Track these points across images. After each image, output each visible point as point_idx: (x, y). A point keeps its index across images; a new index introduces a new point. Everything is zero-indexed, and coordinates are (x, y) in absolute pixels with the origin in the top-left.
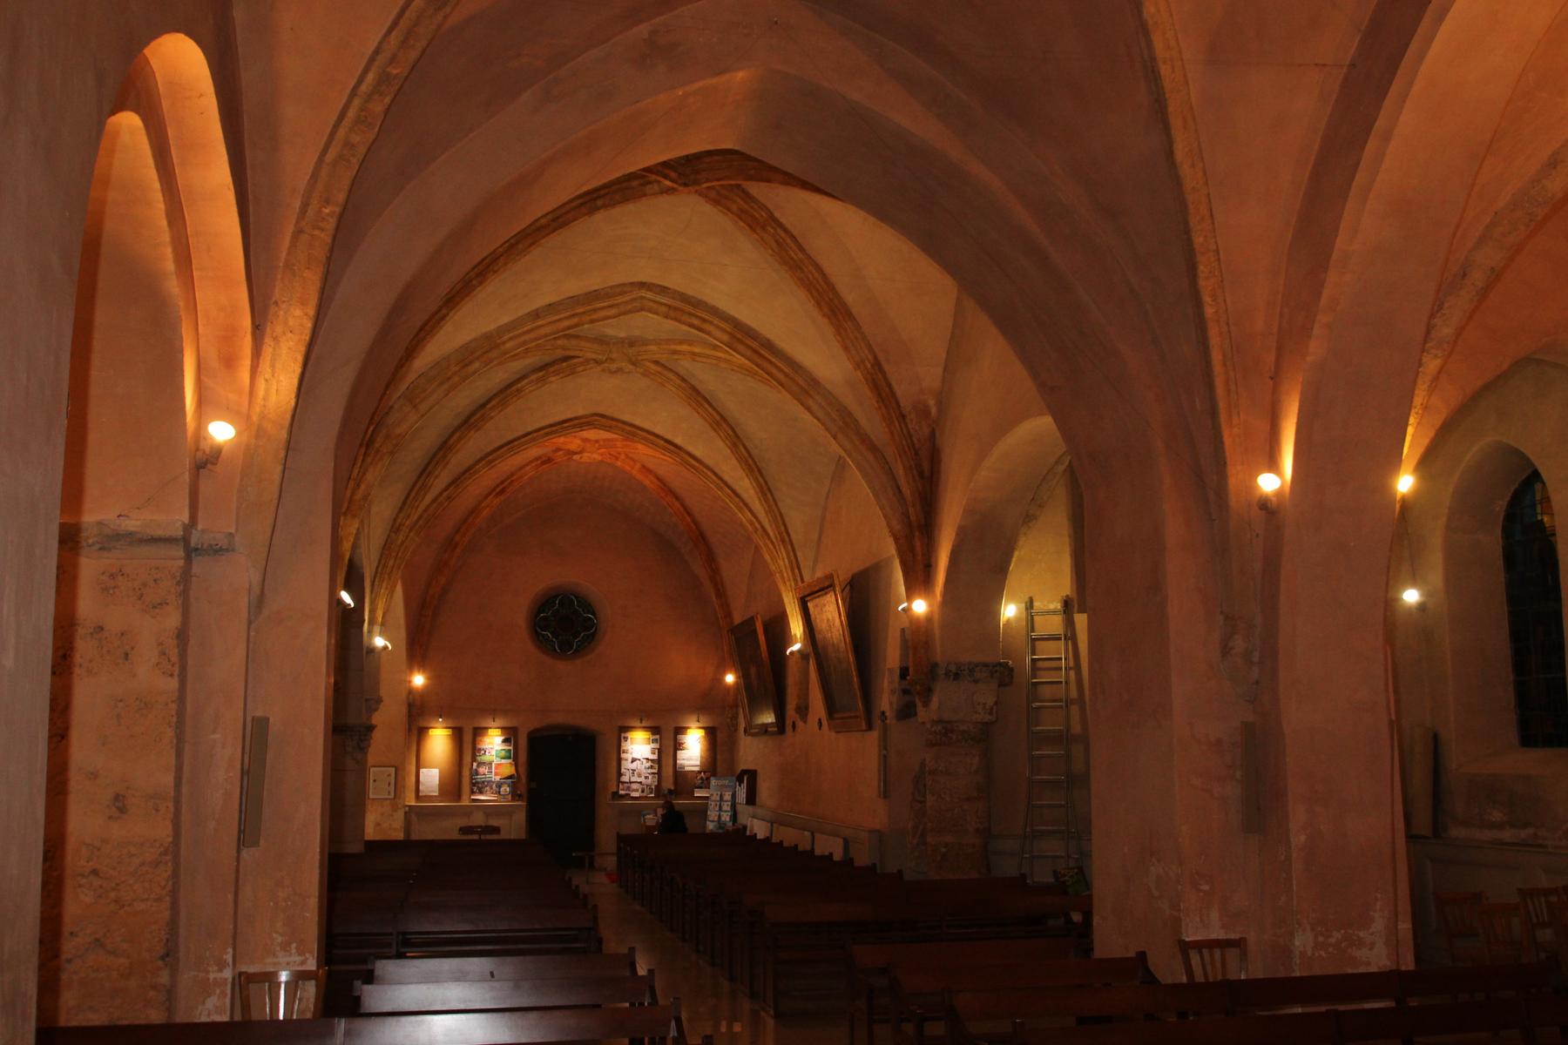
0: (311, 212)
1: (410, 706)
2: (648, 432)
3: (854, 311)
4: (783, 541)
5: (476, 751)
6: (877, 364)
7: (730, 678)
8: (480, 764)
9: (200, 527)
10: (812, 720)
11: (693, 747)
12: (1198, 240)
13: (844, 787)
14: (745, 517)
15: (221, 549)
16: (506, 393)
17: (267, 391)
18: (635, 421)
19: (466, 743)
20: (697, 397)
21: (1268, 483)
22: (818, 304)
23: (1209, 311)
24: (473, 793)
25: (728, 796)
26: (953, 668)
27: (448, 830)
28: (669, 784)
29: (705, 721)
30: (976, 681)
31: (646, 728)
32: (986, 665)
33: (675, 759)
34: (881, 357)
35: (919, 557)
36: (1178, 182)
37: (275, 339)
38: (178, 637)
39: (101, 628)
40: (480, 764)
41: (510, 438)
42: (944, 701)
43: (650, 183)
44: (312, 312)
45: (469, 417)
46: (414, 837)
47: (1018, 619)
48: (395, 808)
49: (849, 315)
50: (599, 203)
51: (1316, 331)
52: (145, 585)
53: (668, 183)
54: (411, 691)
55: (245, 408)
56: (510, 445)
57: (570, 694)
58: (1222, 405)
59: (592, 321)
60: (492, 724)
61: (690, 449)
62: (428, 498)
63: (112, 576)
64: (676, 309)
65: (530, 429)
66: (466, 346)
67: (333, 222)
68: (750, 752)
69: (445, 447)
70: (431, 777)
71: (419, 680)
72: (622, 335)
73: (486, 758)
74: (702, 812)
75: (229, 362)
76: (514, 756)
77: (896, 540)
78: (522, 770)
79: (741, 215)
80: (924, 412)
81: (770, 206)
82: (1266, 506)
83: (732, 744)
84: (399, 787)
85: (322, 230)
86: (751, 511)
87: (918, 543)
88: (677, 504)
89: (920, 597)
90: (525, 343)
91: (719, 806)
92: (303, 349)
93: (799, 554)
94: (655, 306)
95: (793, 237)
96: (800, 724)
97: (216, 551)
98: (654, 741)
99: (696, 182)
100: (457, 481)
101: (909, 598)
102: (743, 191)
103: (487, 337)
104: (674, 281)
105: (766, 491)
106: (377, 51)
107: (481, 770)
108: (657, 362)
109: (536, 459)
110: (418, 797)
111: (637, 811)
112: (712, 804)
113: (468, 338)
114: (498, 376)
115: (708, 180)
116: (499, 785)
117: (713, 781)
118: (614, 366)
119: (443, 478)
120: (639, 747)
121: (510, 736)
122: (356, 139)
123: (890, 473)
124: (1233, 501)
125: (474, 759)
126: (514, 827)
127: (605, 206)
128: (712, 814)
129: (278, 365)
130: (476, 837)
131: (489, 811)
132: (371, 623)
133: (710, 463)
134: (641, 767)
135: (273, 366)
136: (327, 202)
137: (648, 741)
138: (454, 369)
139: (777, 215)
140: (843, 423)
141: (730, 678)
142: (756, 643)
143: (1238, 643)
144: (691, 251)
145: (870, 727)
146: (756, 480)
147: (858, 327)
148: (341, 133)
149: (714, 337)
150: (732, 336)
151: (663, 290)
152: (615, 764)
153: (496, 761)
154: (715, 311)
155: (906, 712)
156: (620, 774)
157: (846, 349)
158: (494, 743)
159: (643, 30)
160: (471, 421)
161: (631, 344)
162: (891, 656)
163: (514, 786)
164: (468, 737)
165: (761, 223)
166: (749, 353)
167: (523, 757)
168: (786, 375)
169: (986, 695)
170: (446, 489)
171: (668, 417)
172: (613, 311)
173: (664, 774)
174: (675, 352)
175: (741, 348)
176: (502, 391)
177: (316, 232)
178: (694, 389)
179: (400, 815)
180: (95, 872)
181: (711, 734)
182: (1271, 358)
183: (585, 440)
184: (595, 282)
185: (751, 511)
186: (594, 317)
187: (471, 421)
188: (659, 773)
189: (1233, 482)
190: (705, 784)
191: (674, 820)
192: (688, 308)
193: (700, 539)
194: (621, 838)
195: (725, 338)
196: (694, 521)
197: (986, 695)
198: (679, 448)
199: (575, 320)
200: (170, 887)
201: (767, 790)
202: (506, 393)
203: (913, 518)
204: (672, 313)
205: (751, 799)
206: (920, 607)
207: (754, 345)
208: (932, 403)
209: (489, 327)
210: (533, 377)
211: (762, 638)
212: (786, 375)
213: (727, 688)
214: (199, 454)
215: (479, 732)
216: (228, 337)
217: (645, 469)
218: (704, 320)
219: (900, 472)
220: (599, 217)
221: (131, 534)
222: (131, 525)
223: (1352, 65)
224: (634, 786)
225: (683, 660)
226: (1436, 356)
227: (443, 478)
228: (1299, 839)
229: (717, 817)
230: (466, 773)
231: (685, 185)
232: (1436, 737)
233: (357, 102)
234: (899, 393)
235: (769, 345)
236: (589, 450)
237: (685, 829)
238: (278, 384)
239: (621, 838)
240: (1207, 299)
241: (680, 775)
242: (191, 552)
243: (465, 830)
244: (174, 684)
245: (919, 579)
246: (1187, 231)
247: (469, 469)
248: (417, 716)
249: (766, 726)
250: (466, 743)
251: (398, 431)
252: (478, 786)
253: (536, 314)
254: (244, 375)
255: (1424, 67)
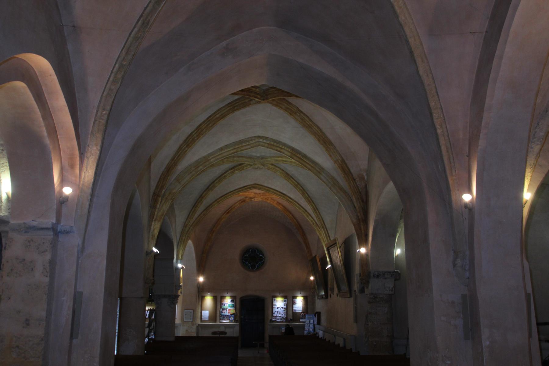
0: (99, 113)
5: (221, 304)
6: (343, 161)
7: (312, 278)
8: (223, 309)
10: (335, 294)
11: (299, 303)
12: (432, 104)
13: (344, 318)
14: (309, 219)
16: (221, 177)
17: (85, 176)
18: (268, 186)
19: (218, 301)
20: (288, 176)
21: (467, 198)
22: (319, 140)
23: (439, 131)
24: (220, 319)
25: (312, 322)
26: (376, 273)
27: (207, 333)
28: (290, 317)
29: (303, 294)
30: (385, 278)
31: (282, 296)
32: (390, 272)
34: (345, 159)
35: (363, 232)
36: (422, 83)
37: (87, 158)
38: (50, 263)
39: (24, 260)
40: (223, 309)
41: (225, 193)
42: (375, 286)
43: (252, 100)
44: (99, 148)
45: (208, 187)
46: (200, 335)
47: (401, 254)
48: (193, 325)
49: (331, 144)
50: (236, 108)
51: (482, 136)
52: (40, 245)
53: (257, 99)
54: (199, 283)
55: (78, 183)
56: (225, 196)
57: (255, 284)
58: (447, 168)
59: (242, 150)
60: (299, 295)
61: (289, 195)
62: (196, 215)
63: (29, 242)
64: (271, 145)
65: (232, 190)
66: (197, 161)
67: (106, 116)
68: (320, 305)
69: (201, 197)
70: (206, 314)
71: (201, 279)
72: (258, 155)
73: (225, 307)
74: (303, 327)
75: (72, 166)
76: (235, 306)
77: (354, 225)
78: (238, 311)
79: (286, 110)
80: (362, 178)
81: (297, 106)
82: (466, 206)
83: (314, 303)
84: (194, 317)
85: (102, 119)
86: (311, 217)
87: (362, 227)
88: (291, 215)
89: (363, 247)
90: (217, 159)
91: (309, 325)
92: (96, 161)
93: (329, 232)
94: (263, 144)
95: (307, 116)
96: (332, 295)
97: (67, 232)
98: (285, 301)
99: (267, 99)
100: (207, 208)
101: (360, 248)
102: (287, 101)
103: (204, 157)
104: (269, 135)
105: (316, 209)
106: (119, 57)
107: (223, 311)
108: (272, 164)
109: (240, 201)
110: (201, 321)
111: (279, 327)
112: (306, 325)
113: (197, 158)
114: (217, 171)
115: (271, 98)
117: (307, 316)
118: (256, 166)
119: (201, 209)
120: (279, 303)
121: (233, 299)
122: (113, 87)
123: (351, 201)
124: (454, 205)
125: (221, 308)
126: (234, 332)
127: (237, 109)
128: (306, 329)
129: (89, 167)
130: (218, 336)
131: (226, 326)
132: (177, 259)
133: (295, 200)
134: (280, 310)
135: (87, 167)
136: (104, 110)
138: (193, 169)
139: (300, 109)
140: (333, 183)
141: (312, 278)
142: (316, 264)
143: (459, 262)
144: (267, 122)
145: (351, 296)
146: (312, 205)
149: (282, 154)
150: (292, 153)
151: (266, 138)
152: (271, 309)
153: (229, 308)
154: (285, 145)
155: (362, 291)
156: (273, 313)
157: (330, 156)
159: (224, 44)
160: (210, 187)
161: (262, 158)
162: (357, 269)
163: (235, 317)
164: (219, 299)
165: (295, 112)
166: (298, 159)
167: (238, 306)
168: (312, 167)
169: (390, 284)
170: (203, 212)
171: (279, 184)
172: (249, 147)
173: (289, 313)
174: (277, 160)
175: (295, 158)
176: (220, 177)
177: (101, 120)
178: (288, 174)
179: (195, 327)
180: (18, 347)
181: (306, 298)
182: (467, 149)
183: (256, 193)
184: (242, 137)
185: (311, 217)
186: (242, 149)
187: (210, 187)
188: (287, 313)
189: (454, 198)
190: (304, 317)
191: (289, 330)
192: (275, 144)
193: (299, 227)
194: (269, 336)
195: (289, 154)
196: (297, 221)
197: (390, 284)
199: (235, 150)
201: (323, 318)
202: (221, 177)
203: (360, 217)
204: (270, 146)
205: (319, 323)
206: (363, 250)
207: (299, 156)
208: (365, 174)
209: (205, 154)
211: (319, 263)
212: (312, 167)
213: (311, 281)
214: (61, 199)
215: (223, 298)
216: (71, 158)
217: (278, 203)
218: (281, 148)
219: (354, 200)
220: (237, 113)
221: (34, 227)
222: (35, 224)
223: (487, 32)
224: (278, 318)
225: (294, 271)
226: (538, 144)
227: (201, 209)
228: (486, 343)
229: (309, 328)
230: (218, 312)
231: (264, 100)
233: (113, 75)
235: (305, 156)
236: (256, 196)
238: (88, 174)
239: (269, 336)
240: (438, 127)
241: (294, 313)
242: (57, 233)
243: (214, 333)
244: (47, 279)
245: (363, 241)
246: (428, 101)
247: (211, 205)
249: (322, 295)
250: (218, 301)
251: (174, 191)
252: (223, 317)
253: (221, 149)
254: (77, 171)
255: (512, 30)
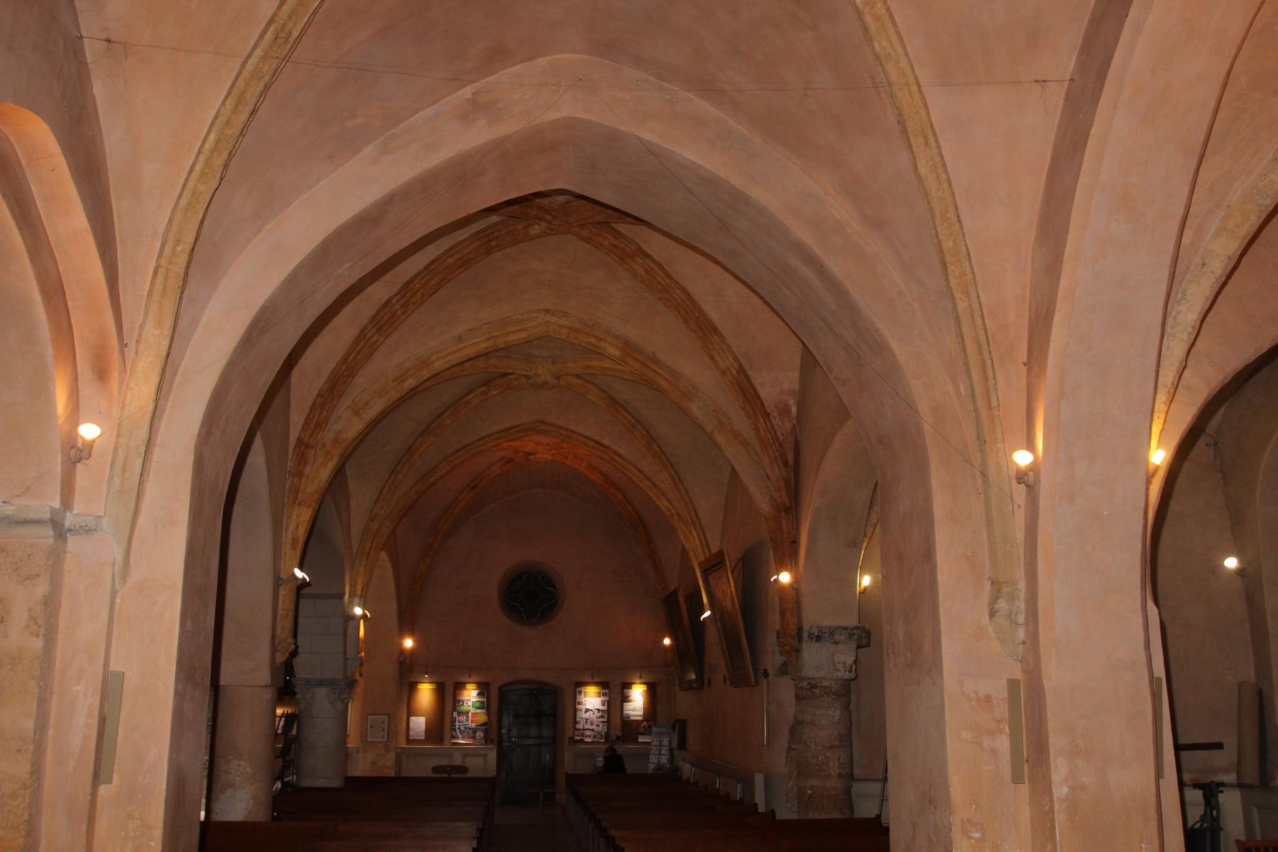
1: (401, 664)
2: (581, 435)
3: (720, 328)
4: (693, 523)
5: (456, 702)
6: (741, 370)
7: (667, 641)
8: (460, 713)
9: (75, 512)
11: (637, 697)
12: (948, 245)
15: (90, 530)
19: (447, 696)
24: (453, 737)
27: (422, 769)
28: (616, 731)
31: (597, 684)
32: (846, 628)
33: (622, 709)
38: (45, 604)
40: (460, 713)
46: (403, 774)
49: (715, 330)
54: (402, 651)
57: (537, 653)
60: (638, 681)
68: (685, 703)
70: (419, 723)
71: (408, 643)
73: (465, 708)
76: (485, 705)
95: (659, 265)
98: (604, 694)
116: (474, 731)
117: (654, 729)
120: (591, 700)
121: (483, 689)
125: (454, 709)
128: (653, 759)
131: (466, 752)
132: (352, 595)
137: (599, 695)
141: (667, 641)
147: (723, 340)
148: (190, 184)
153: (472, 710)
156: (576, 723)
158: (471, 695)
159: (467, 91)
163: (486, 733)
179: (392, 755)
183: (539, 443)
188: (608, 722)
190: (648, 732)
191: (614, 762)
198: (607, 448)
200: (26, 817)
205: (682, 744)
210: (479, 391)
211: (684, 607)
215: (460, 686)
223: (1072, 80)
224: (588, 733)
232: (1260, 693)
233: (202, 158)
234: (762, 393)
237: (623, 770)
243: (435, 769)
244: (38, 643)
248: (407, 672)
250: (447, 696)
